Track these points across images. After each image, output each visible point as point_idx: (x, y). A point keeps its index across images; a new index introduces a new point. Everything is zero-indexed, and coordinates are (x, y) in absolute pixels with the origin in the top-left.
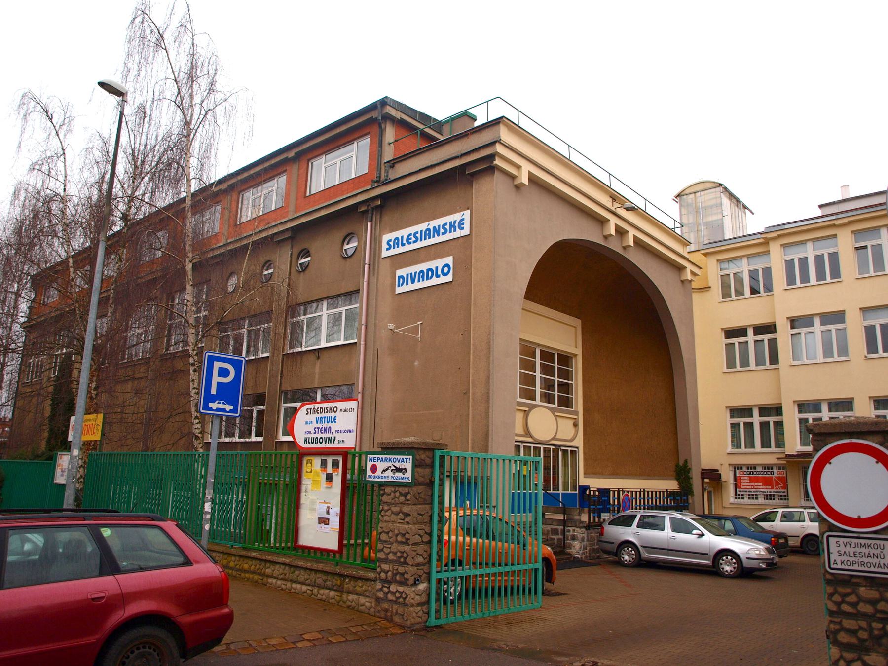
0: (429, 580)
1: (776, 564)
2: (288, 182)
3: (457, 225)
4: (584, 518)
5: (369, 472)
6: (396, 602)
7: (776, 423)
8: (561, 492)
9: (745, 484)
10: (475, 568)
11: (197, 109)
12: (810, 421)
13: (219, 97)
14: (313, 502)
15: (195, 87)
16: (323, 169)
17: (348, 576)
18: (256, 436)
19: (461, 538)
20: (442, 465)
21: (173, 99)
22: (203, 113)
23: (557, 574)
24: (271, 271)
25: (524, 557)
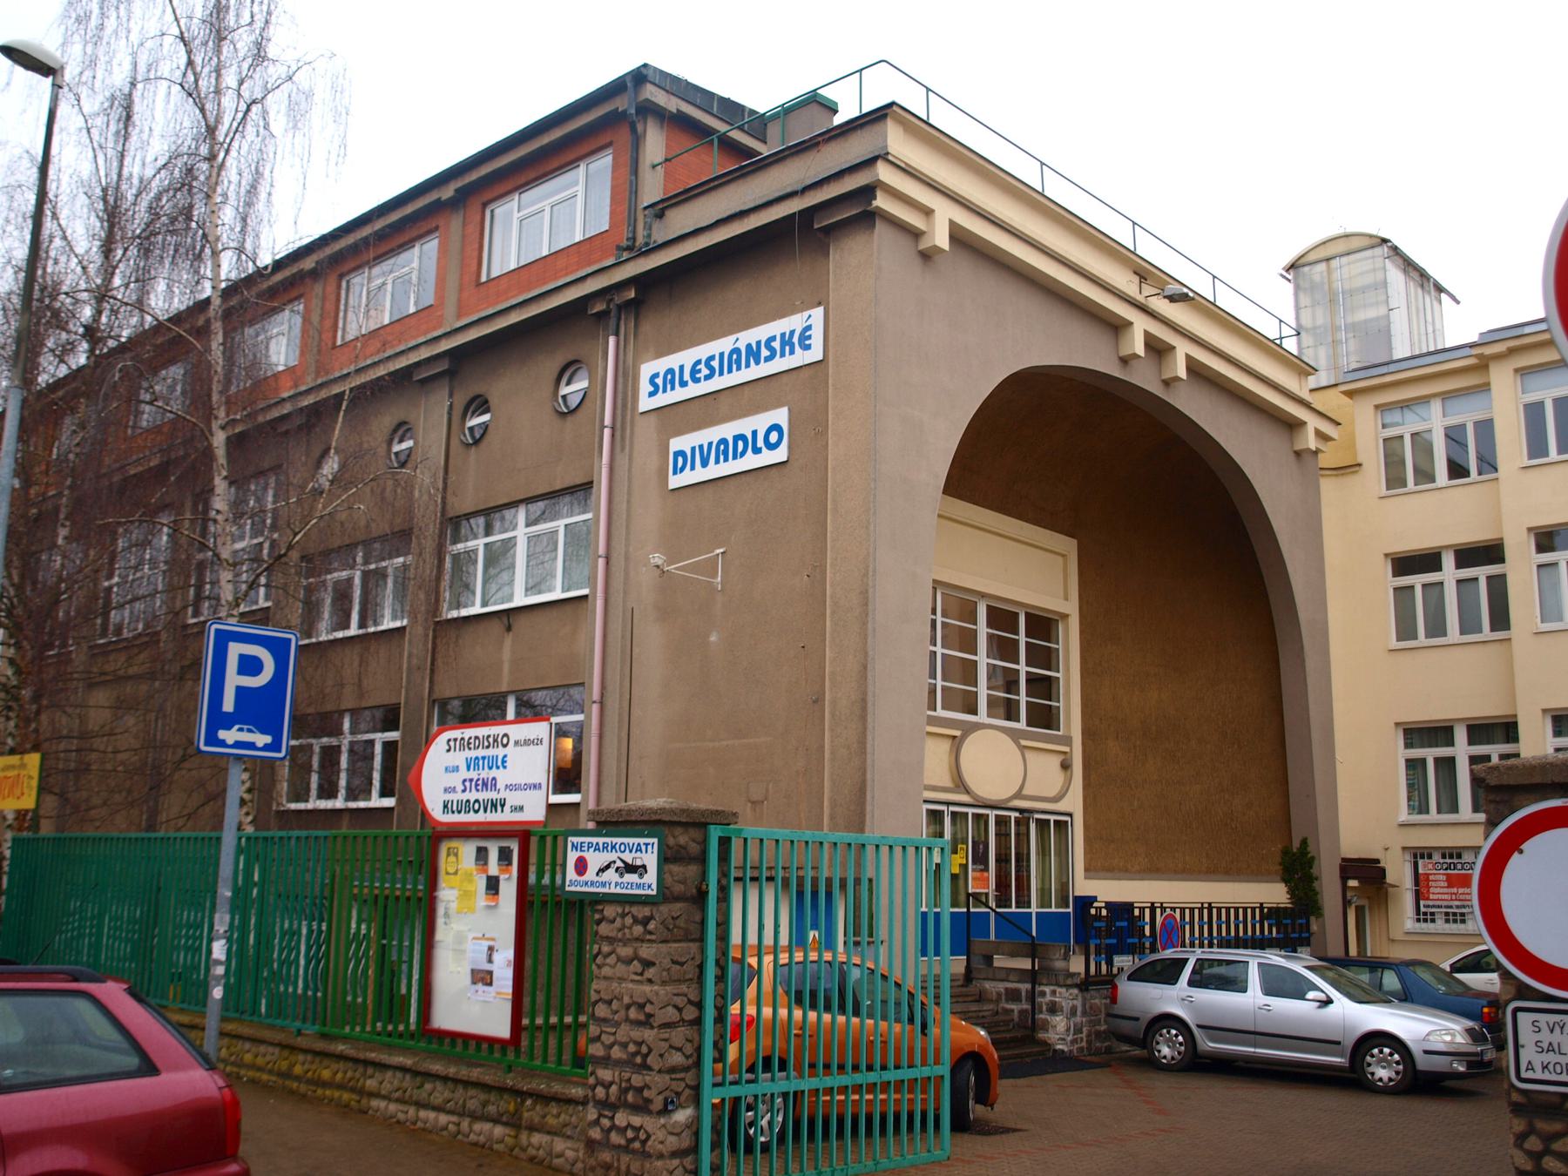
0: (697, 1101)
1: (1490, 1063)
2: (443, 251)
3: (795, 340)
4: (1077, 965)
5: (571, 873)
6: (626, 1149)
8: (1034, 909)
9: (1439, 891)
10: (801, 1076)
11: (228, 101)
12: (1495, 760)
13: (274, 72)
14: (460, 939)
15: (226, 49)
16: (515, 223)
17: (530, 1094)
18: (320, 797)
19: (783, 1013)
20: (724, 857)
21: (178, 75)
22: (243, 107)
23: (1005, 1088)
24: (404, 446)
25: (924, 1051)
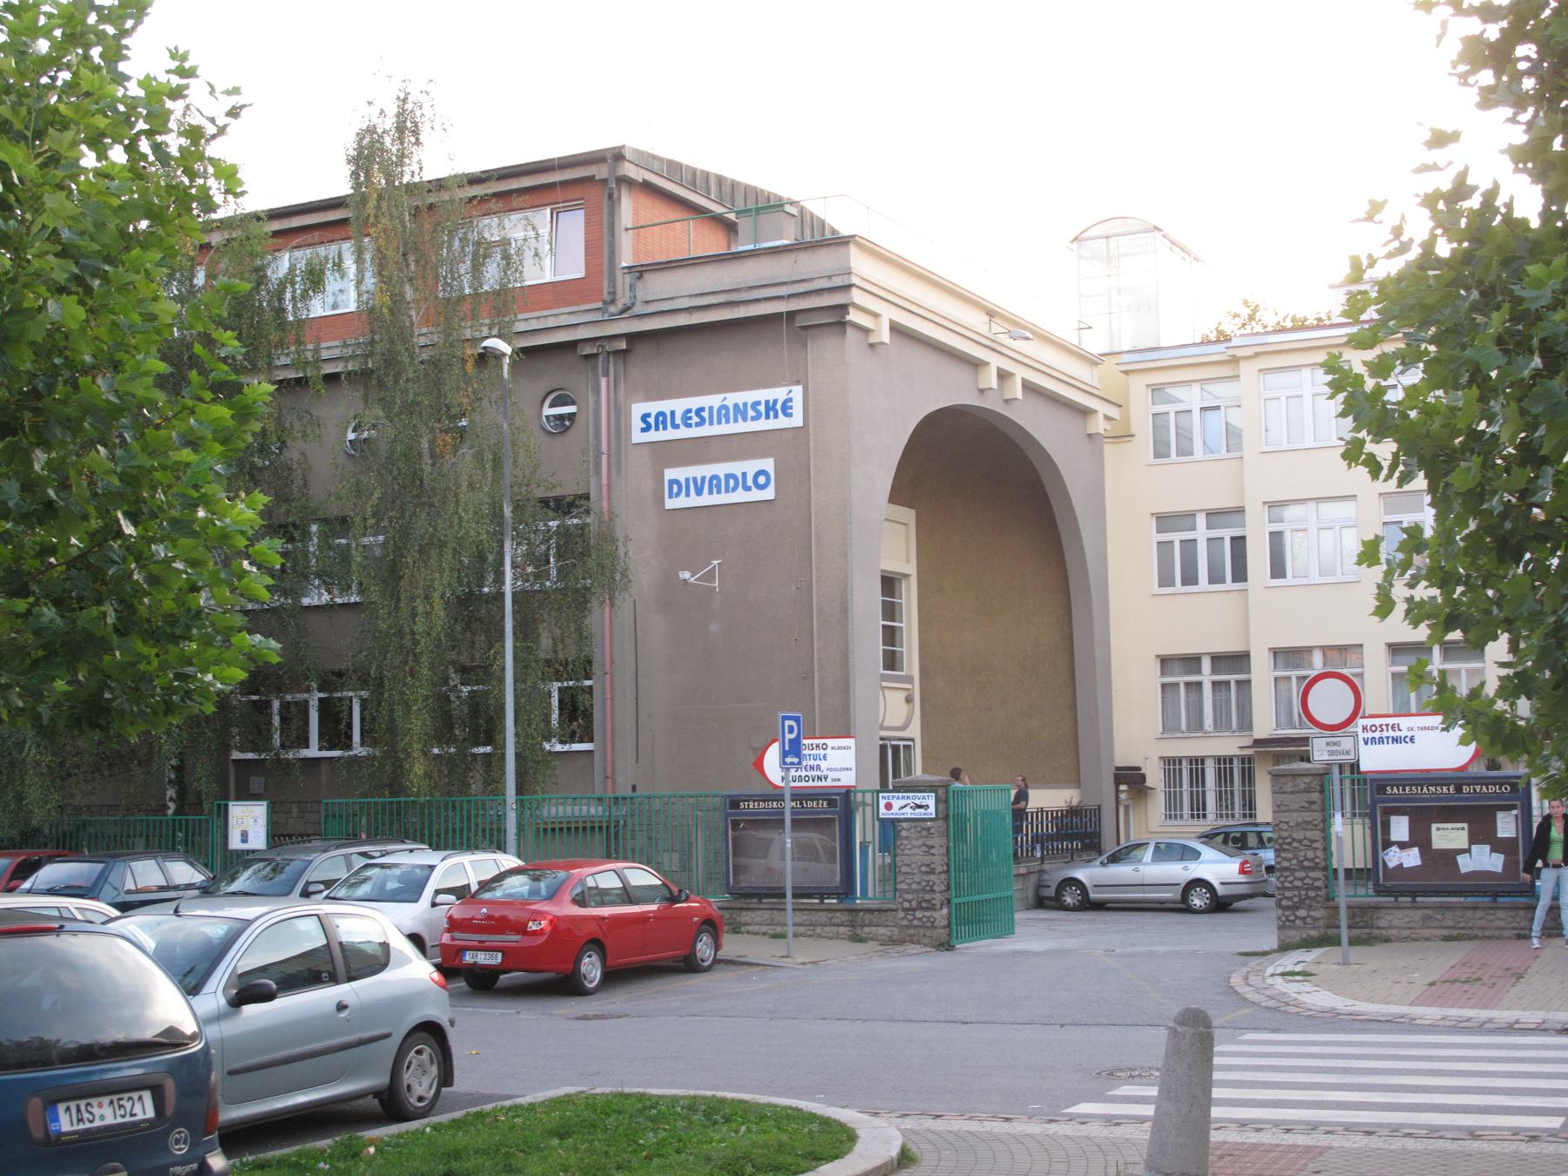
3: (779, 407)
7: (1238, 682)
